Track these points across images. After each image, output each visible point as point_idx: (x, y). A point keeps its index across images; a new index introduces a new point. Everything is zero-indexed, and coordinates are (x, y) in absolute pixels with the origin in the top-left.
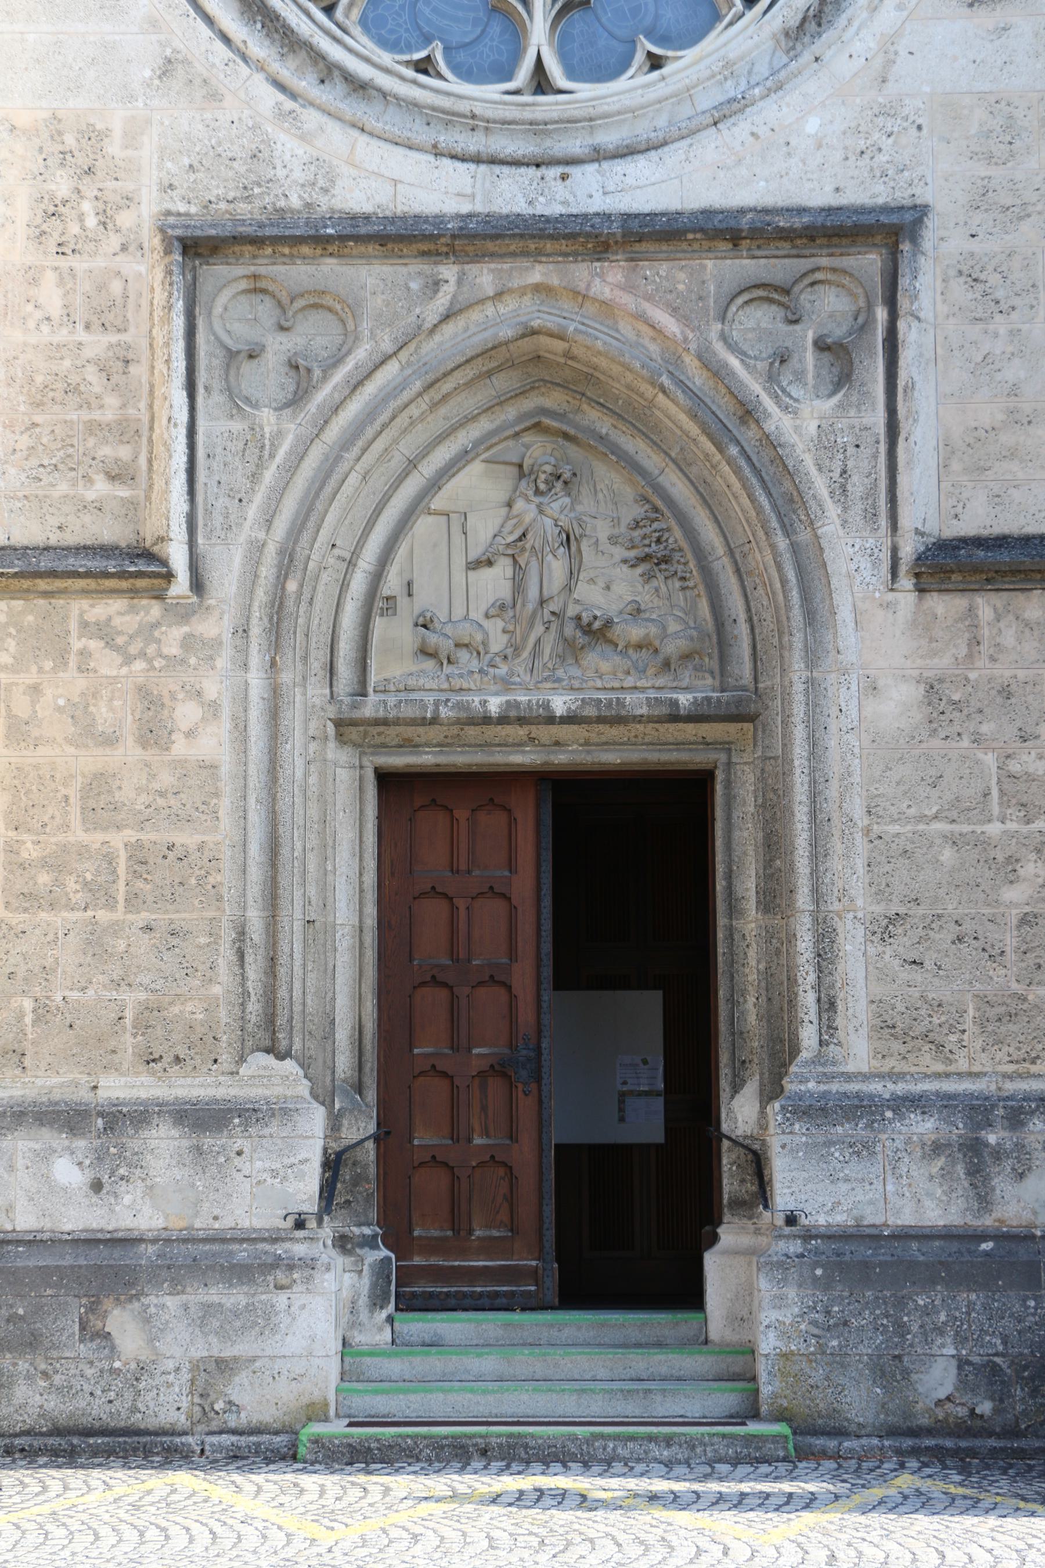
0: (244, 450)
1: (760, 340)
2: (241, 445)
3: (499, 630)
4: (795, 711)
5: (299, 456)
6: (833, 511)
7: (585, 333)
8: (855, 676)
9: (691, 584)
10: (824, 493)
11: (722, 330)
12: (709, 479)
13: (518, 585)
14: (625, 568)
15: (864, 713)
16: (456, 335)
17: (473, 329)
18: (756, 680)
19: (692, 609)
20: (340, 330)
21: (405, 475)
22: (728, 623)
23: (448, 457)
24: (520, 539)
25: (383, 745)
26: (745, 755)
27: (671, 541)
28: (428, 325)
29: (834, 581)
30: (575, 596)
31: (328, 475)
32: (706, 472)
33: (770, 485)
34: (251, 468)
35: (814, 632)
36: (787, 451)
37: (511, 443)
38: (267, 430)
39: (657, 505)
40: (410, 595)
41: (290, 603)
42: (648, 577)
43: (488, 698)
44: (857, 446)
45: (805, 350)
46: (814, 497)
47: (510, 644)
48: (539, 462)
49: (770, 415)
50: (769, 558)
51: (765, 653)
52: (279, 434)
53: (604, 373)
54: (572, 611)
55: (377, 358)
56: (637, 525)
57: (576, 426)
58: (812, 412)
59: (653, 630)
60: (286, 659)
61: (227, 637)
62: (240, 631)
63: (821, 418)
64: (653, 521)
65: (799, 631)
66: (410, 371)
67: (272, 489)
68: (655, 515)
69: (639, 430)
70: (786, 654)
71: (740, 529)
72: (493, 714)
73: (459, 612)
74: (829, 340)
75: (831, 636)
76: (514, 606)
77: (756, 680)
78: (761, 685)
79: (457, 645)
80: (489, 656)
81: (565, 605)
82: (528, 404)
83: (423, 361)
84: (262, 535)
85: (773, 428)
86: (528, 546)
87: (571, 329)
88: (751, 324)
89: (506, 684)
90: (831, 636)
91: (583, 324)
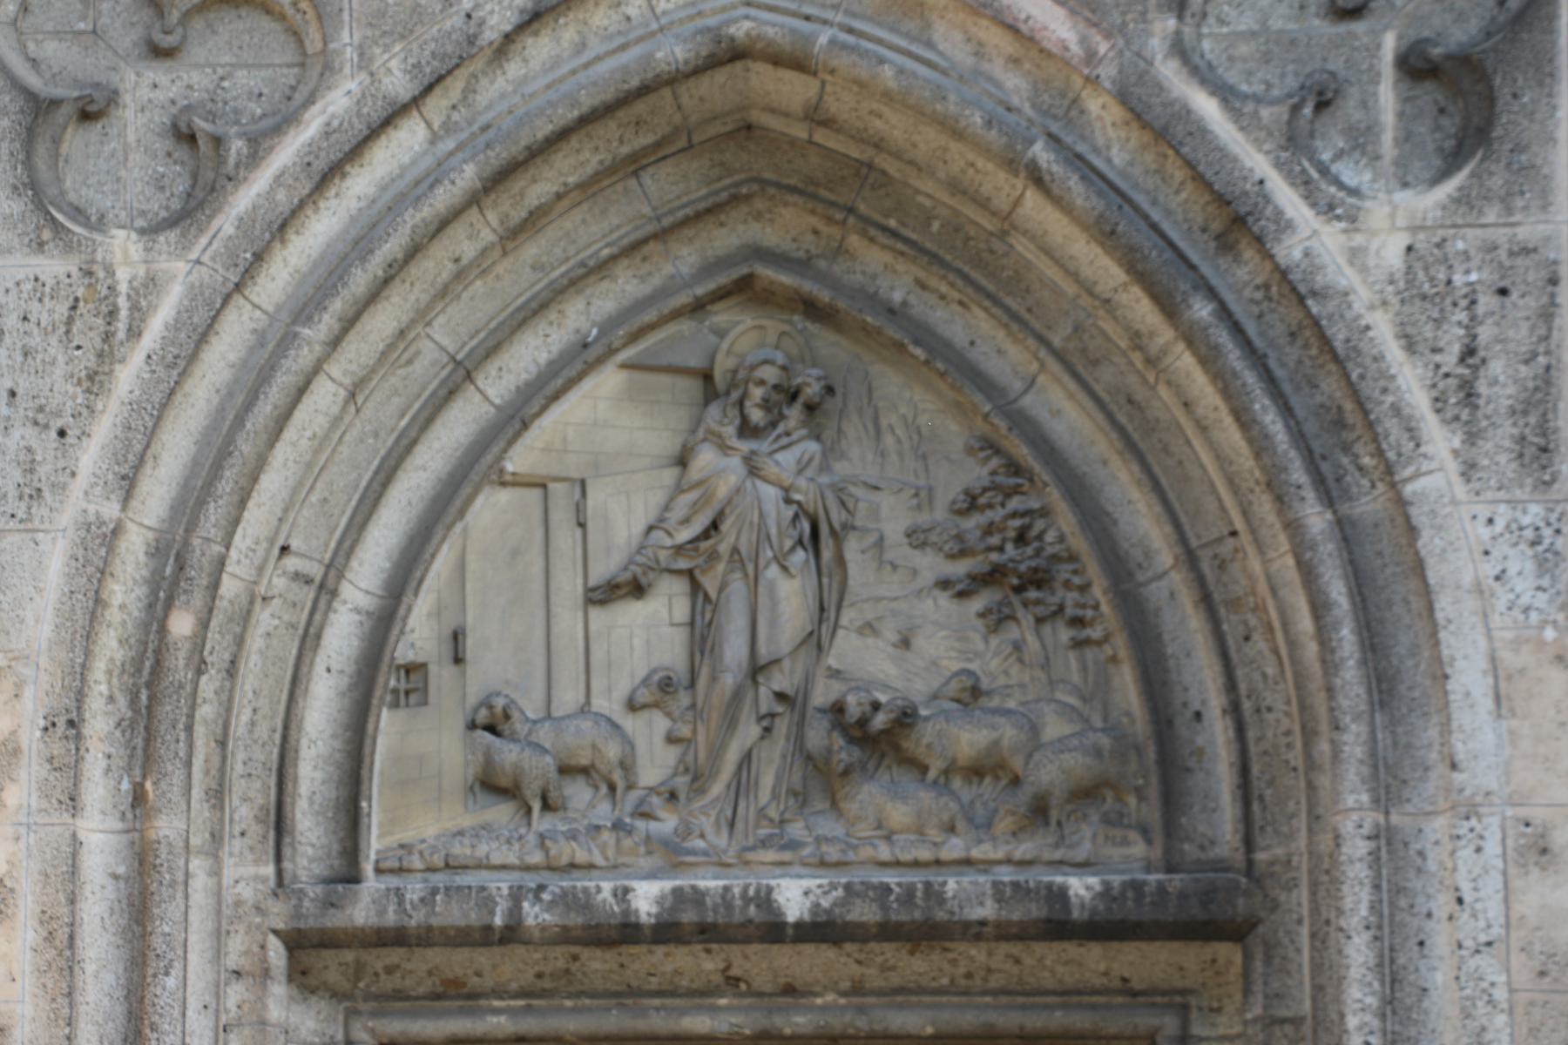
0: (70, 321)
1: (1266, 58)
2: (62, 309)
3: (659, 738)
4: (1348, 903)
5: (197, 334)
6: (1441, 441)
7: (853, 49)
8: (1495, 821)
9: (1095, 633)
10: (1419, 400)
11: (1178, 33)
12: (1141, 395)
13: (702, 637)
14: (944, 599)
15: (1518, 909)
16: (556, 62)
17: (596, 47)
18: (1249, 844)
19: (1098, 691)
20: (290, 56)
21: (447, 394)
22: (1182, 721)
23: (543, 357)
24: (705, 535)
25: (399, 995)
26: (1222, 1019)
27: (1050, 537)
28: (491, 35)
29: (1444, 606)
30: (832, 661)
31: (265, 376)
32: (1132, 379)
33: (1287, 388)
34: (87, 360)
35: (1393, 723)
36: (1331, 306)
37: (685, 326)
38: (123, 275)
39: (1017, 461)
40: (458, 660)
41: (178, 662)
42: (997, 619)
43: (635, 884)
44: (1503, 292)
45: (1375, 78)
46: (1396, 410)
47: (683, 767)
48: (750, 360)
49: (1289, 226)
50: (1286, 565)
51: (1271, 783)
52: (151, 284)
53: (897, 155)
54: (823, 694)
55: (374, 111)
56: (971, 503)
57: (836, 286)
58: (1392, 216)
59: (1009, 733)
60: (165, 788)
61: (30, 738)
62: (61, 722)
63: (1414, 229)
64: (1010, 493)
65: (1357, 718)
66: (450, 144)
67: (135, 407)
68: (1013, 481)
69: (978, 288)
70: (1324, 781)
71: (1210, 505)
72: (644, 918)
73: (568, 697)
74: (1436, 52)
75: (1433, 733)
76: (692, 684)
77: (1249, 844)
78: (1261, 856)
79: (565, 770)
80: (634, 795)
81: (808, 680)
82: (726, 237)
83: (482, 120)
84: (111, 510)
85: (1297, 254)
86: (724, 548)
87: (823, 40)
88: (1246, 23)
89: (673, 855)
90: (1433, 733)
91: (850, 31)
